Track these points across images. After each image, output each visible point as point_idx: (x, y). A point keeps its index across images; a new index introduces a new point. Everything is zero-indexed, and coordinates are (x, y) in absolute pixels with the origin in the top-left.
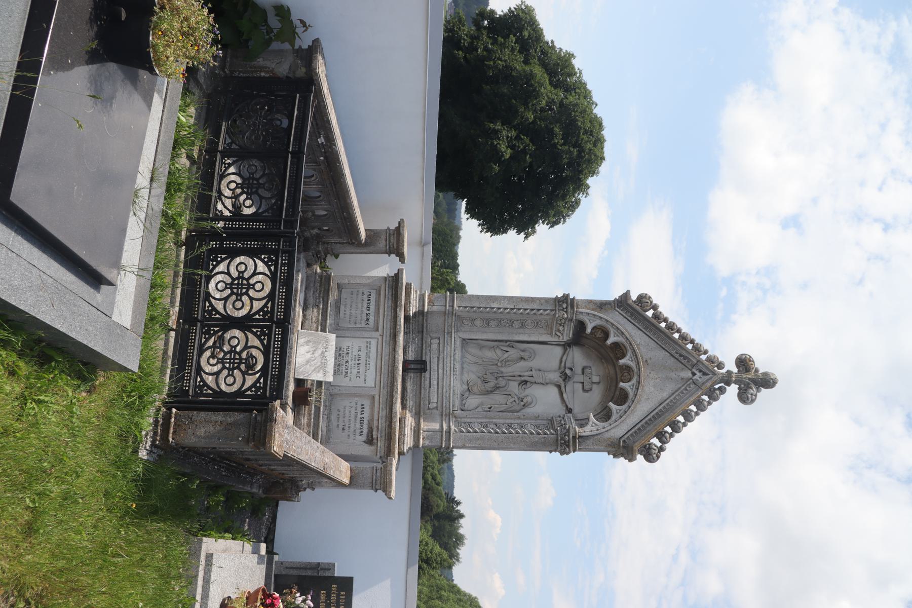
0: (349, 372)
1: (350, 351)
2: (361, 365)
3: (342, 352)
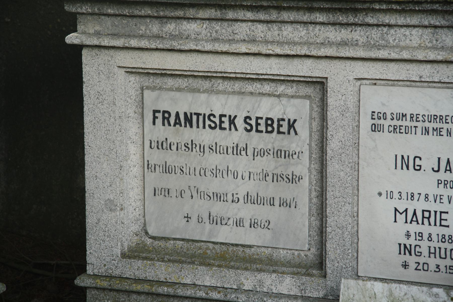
3: (425, 244)
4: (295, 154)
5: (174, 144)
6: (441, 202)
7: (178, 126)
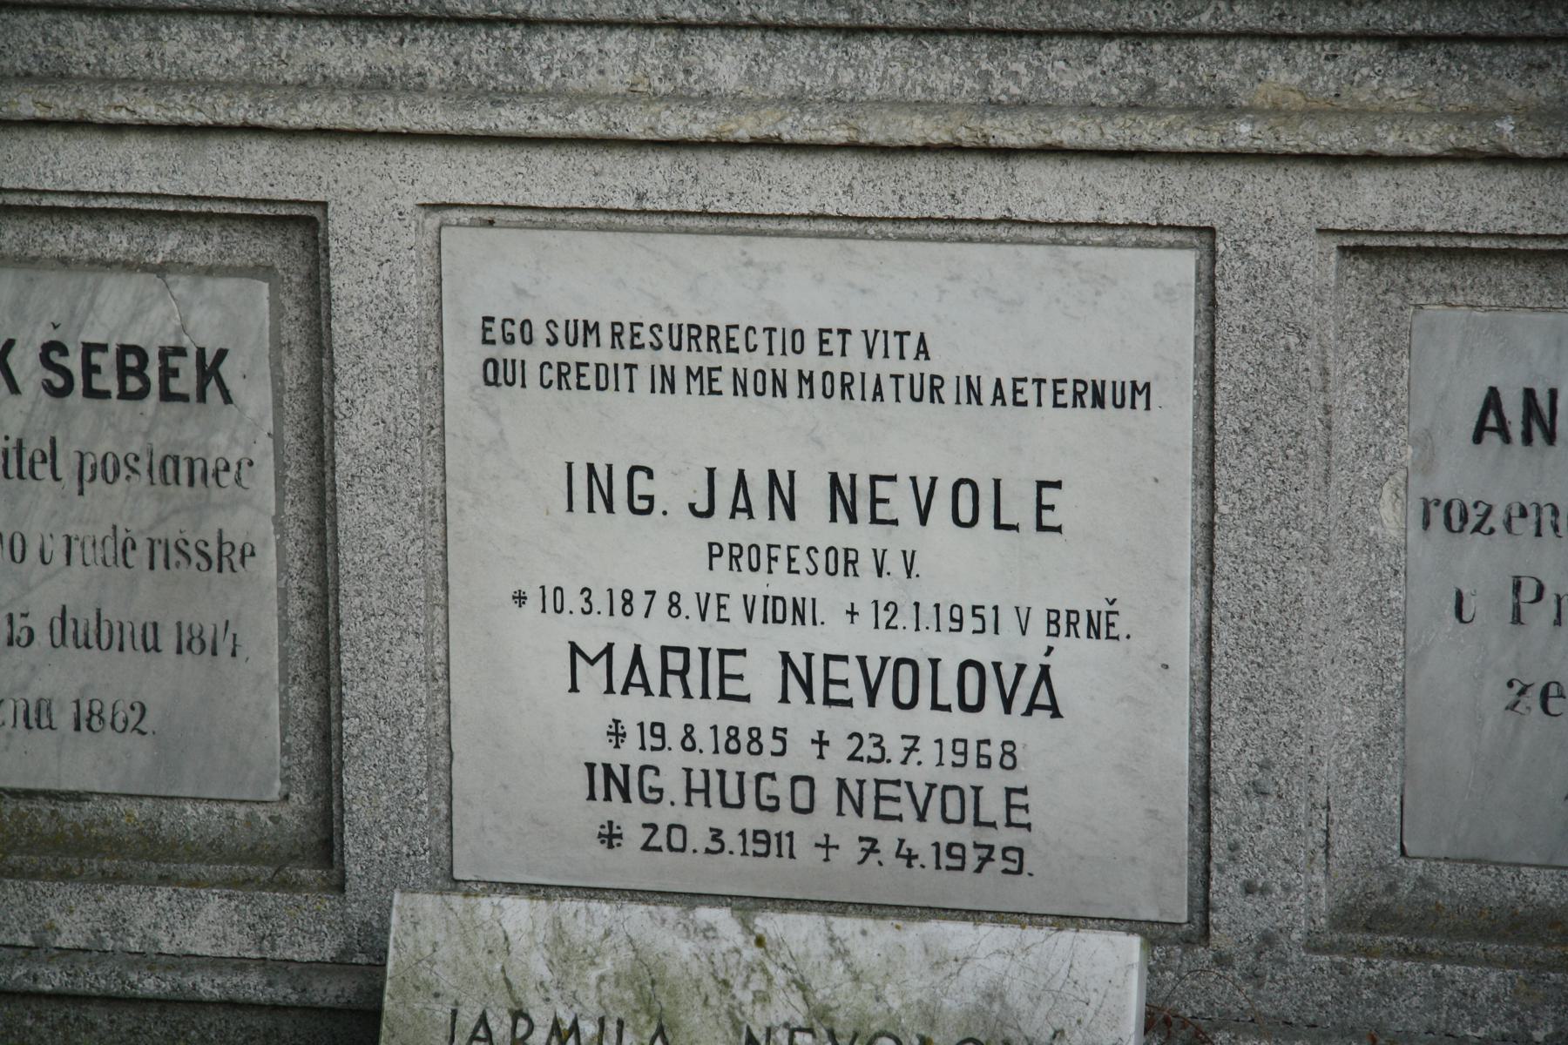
0: (969, 645)
1: (653, 632)
2: (857, 463)
3: (672, 763)
4: (227, 469)
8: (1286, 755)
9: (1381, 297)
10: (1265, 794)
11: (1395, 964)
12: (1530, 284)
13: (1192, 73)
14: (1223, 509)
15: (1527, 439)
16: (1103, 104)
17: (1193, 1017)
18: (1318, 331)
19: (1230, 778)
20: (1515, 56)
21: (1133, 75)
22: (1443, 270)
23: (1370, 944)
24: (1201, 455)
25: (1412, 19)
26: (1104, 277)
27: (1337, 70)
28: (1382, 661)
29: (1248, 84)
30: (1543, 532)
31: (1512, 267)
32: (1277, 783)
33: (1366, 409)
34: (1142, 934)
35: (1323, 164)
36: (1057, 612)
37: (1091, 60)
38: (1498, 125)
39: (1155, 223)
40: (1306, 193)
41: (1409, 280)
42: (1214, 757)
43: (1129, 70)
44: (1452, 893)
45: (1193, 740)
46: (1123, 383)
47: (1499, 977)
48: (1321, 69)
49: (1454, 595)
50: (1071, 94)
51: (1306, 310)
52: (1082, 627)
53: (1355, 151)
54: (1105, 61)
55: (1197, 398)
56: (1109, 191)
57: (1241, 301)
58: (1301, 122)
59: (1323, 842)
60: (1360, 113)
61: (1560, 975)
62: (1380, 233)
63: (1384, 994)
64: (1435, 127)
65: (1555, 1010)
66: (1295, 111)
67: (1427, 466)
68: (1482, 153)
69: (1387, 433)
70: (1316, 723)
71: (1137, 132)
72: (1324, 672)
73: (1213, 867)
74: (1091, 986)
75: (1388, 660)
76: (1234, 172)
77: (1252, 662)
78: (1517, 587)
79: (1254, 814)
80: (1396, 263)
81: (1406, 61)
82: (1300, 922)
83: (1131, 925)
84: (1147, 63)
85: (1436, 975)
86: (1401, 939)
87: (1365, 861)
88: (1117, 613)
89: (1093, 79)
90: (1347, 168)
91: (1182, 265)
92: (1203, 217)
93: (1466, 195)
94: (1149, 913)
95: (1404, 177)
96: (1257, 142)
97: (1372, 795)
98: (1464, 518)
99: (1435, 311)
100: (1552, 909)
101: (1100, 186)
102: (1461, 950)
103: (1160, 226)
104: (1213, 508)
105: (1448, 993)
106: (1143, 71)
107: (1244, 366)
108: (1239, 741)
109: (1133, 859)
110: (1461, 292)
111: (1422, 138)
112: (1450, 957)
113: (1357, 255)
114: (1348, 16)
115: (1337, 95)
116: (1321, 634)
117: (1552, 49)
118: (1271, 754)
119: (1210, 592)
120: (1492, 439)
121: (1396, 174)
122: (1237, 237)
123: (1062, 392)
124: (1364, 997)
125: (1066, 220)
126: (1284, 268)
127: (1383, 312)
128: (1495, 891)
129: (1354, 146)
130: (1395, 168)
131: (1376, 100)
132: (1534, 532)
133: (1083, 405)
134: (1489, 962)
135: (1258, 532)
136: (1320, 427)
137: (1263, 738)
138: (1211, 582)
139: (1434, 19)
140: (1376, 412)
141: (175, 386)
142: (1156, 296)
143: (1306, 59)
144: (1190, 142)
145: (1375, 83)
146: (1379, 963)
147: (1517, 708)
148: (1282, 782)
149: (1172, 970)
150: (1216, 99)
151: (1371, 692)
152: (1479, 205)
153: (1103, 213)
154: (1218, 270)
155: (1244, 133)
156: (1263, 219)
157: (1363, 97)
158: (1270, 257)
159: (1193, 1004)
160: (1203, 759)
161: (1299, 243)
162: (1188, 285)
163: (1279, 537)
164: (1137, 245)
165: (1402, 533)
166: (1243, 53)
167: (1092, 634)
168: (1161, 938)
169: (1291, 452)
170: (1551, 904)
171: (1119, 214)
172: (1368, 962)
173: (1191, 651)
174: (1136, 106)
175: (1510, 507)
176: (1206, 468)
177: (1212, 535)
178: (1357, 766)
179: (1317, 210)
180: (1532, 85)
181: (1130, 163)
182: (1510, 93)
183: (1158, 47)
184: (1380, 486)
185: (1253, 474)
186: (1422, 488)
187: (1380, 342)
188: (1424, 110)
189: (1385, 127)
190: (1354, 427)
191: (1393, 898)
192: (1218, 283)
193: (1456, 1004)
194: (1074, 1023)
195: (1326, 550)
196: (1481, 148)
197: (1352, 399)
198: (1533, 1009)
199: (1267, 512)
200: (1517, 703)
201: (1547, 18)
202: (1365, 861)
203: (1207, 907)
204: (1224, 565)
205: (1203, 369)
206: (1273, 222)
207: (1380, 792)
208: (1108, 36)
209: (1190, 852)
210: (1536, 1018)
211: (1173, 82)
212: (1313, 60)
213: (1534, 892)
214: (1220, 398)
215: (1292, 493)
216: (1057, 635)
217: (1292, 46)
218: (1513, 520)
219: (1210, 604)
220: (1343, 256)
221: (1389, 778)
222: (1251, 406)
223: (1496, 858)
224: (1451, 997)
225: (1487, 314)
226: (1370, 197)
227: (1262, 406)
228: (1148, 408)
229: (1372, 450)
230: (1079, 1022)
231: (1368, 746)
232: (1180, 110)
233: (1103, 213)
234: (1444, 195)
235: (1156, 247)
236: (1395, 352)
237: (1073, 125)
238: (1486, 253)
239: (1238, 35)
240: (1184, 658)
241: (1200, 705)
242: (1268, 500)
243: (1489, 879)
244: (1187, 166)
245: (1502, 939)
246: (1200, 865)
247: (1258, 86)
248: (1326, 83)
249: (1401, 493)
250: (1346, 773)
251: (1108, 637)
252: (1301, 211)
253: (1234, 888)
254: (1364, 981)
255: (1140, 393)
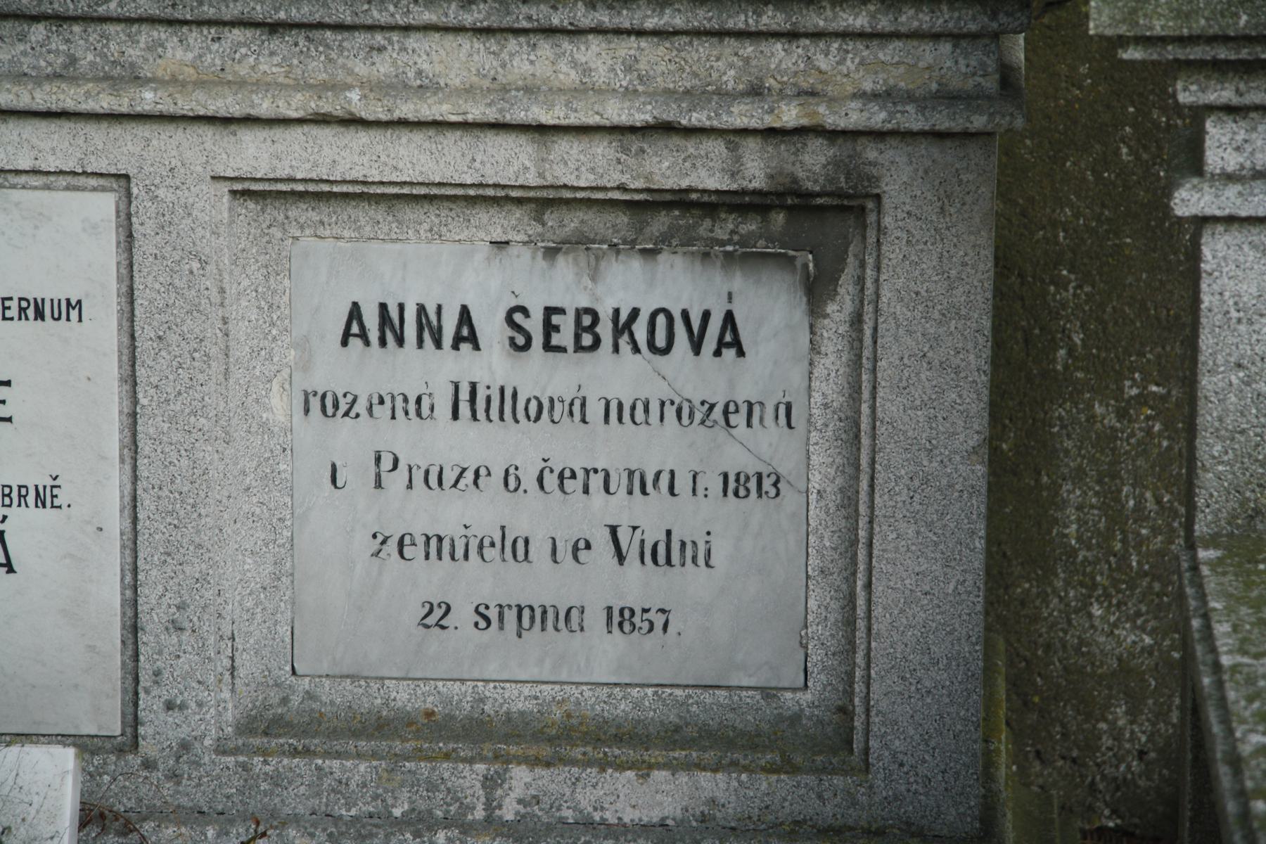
4: (382, 402)
5: (737, 411)
6: (55, 504)
7: (465, 347)
8: (198, 598)
9: (266, 231)
10: (181, 629)
11: (286, 761)
12: (381, 220)
13: (105, 50)
14: (143, 401)
15: (383, 342)
16: (34, 74)
17: (125, 811)
18: (215, 258)
19: (153, 621)
20: (360, 40)
21: (57, 52)
22: (313, 209)
23: (267, 746)
24: (125, 358)
25: (277, 10)
26: (41, 214)
27: (221, 50)
28: (274, 520)
29: (151, 60)
30: (397, 415)
31: (367, 207)
32: (191, 621)
33: (257, 320)
34: (75, 745)
35: (214, 124)
36: (10, 487)
37: (22, 38)
38: (348, 95)
39: (80, 171)
40: (201, 148)
41: (287, 218)
42: (140, 601)
43: (54, 46)
44: (332, 703)
45: (123, 588)
46: (59, 300)
47: (366, 768)
48: (208, 48)
49: (330, 467)
50: (6, 66)
51: (205, 241)
52: (31, 499)
53: (237, 114)
54: (33, 39)
55: (121, 311)
56: (42, 145)
57: (153, 234)
58: (194, 91)
59: (229, 666)
60: (241, 84)
61: (413, 764)
62: (261, 180)
63: (278, 785)
64: (299, 96)
65: (410, 791)
66: (189, 82)
67: (306, 366)
68: (337, 117)
69: (274, 339)
70: (222, 571)
71: (62, 97)
72: (228, 530)
73: (140, 690)
74: (35, 789)
75: (279, 519)
76: (144, 130)
77: (170, 524)
78: (378, 460)
79: (173, 646)
80: (277, 204)
81: (275, 43)
82: (210, 731)
83: (62, 739)
84: (68, 41)
85: (319, 768)
86: (291, 741)
87: (264, 680)
88: (59, 487)
89: (24, 53)
90: (233, 127)
91: (104, 205)
92: (119, 166)
93: (326, 150)
94: (89, 729)
95: (278, 136)
96: (159, 106)
97: (269, 628)
98: (691, 415)
99: (307, 242)
100: (408, 712)
101: (35, 141)
102: (338, 747)
103: (84, 173)
104: (135, 401)
105: (327, 782)
106: (65, 47)
107: (157, 286)
108: (160, 588)
109: (76, 686)
110: (327, 227)
111: (289, 104)
112: (329, 753)
113: (246, 197)
114: (227, 7)
115: (222, 70)
116: (225, 500)
117: (387, 35)
118: (186, 597)
119: (135, 468)
120: (355, 343)
121: (272, 132)
122: (147, 182)
123: (9, 308)
124: (262, 788)
125: (7, 168)
126: (186, 207)
127: (268, 242)
128: (365, 700)
129: (237, 111)
130: (271, 128)
131: (253, 74)
132: (390, 416)
133: (27, 319)
134: (359, 756)
135: (172, 420)
136: (220, 335)
137: (179, 585)
138: (136, 460)
139: (294, 11)
140: (265, 322)
141: (556, 340)
142: (84, 230)
143: (196, 40)
144: (105, 105)
145: (251, 60)
146: (273, 761)
147: (380, 555)
148: (195, 619)
149: (108, 774)
150: (125, 71)
151: (267, 545)
152: (337, 158)
153: (38, 163)
154: (133, 209)
155: (148, 99)
156: (168, 168)
157: (243, 70)
158: (174, 198)
159: (125, 801)
160: (132, 604)
161: (198, 187)
162: (110, 221)
163: (189, 423)
164: (67, 188)
165: (288, 418)
166: (146, 35)
167: (39, 504)
168: (100, 748)
169: (196, 355)
170: (408, 708)
171: (51, 164)
172: (265, 761)
173: (121, 516)
174: (61, 76)
175: (371, 396)
176: (129, 368)
177: (135, 423)
178: (256, 605)
179: (211, 161)
180: (374, 64)
181: (58, 122)
182: (357, 70)
183: (77, 29)
184: (270, 381)
185: (167, 372)
186: (303, 382)
187: (266, 267)
188: (291, 82)
189: (260, 96)
190: (248, 335)
191: (286, 708)
192: (134, 219)
193: (333, 790)
194: (19, 821)
195: (227, 433)
196: (335, 113)
197: (245, 312)
198: (393, 792)
199: (179, 403)
200: (380, 550)
201: (381, 11)
202: (264, 680)
203: (136, 722)
204: (145, 446)
205: (124, 289)
206: (176, 170)
207: (275, 625)
208: (36, 19)
209: (122, 678)
210: (395, 798)
211: (90, 57)
212: (202, 42)
213: (394, 700)
214: (138, 312)
215: (199, 388)
216: (10, 506)
217: (185, 29)
218: (374, 407)
219: (135, 478)
220: (235, 199)
221: (282, 613)
222: (164, 318)
223: (365, 674)
224: (330, 785)
225: (349, 244)
226: (252, 151)
227: (172, 318)
228: (80, 320)
229: (263, 353)
230: (23, 820)
231: (265, 589)
232: (96, 79)
233: (38, 163)
234: (309, 150)
235: (83, 190)
236: (278, 275)
237: (8, 91)
238: (346, 196)
239: (141, 20)
240: (115, 523)
241: (129, 560)
242: (180, 393)
243: (361, 691)
244: (104, 125)
245: (370, 737)
246: (130, 689)
247: (159, 61)
248: (213, 59)
249: (287, 386)
250: (248, 611)
251: (53, 507)
252: (198, 162)
253: (158, 705)
254: (262, 776)
255: (74, 308)
